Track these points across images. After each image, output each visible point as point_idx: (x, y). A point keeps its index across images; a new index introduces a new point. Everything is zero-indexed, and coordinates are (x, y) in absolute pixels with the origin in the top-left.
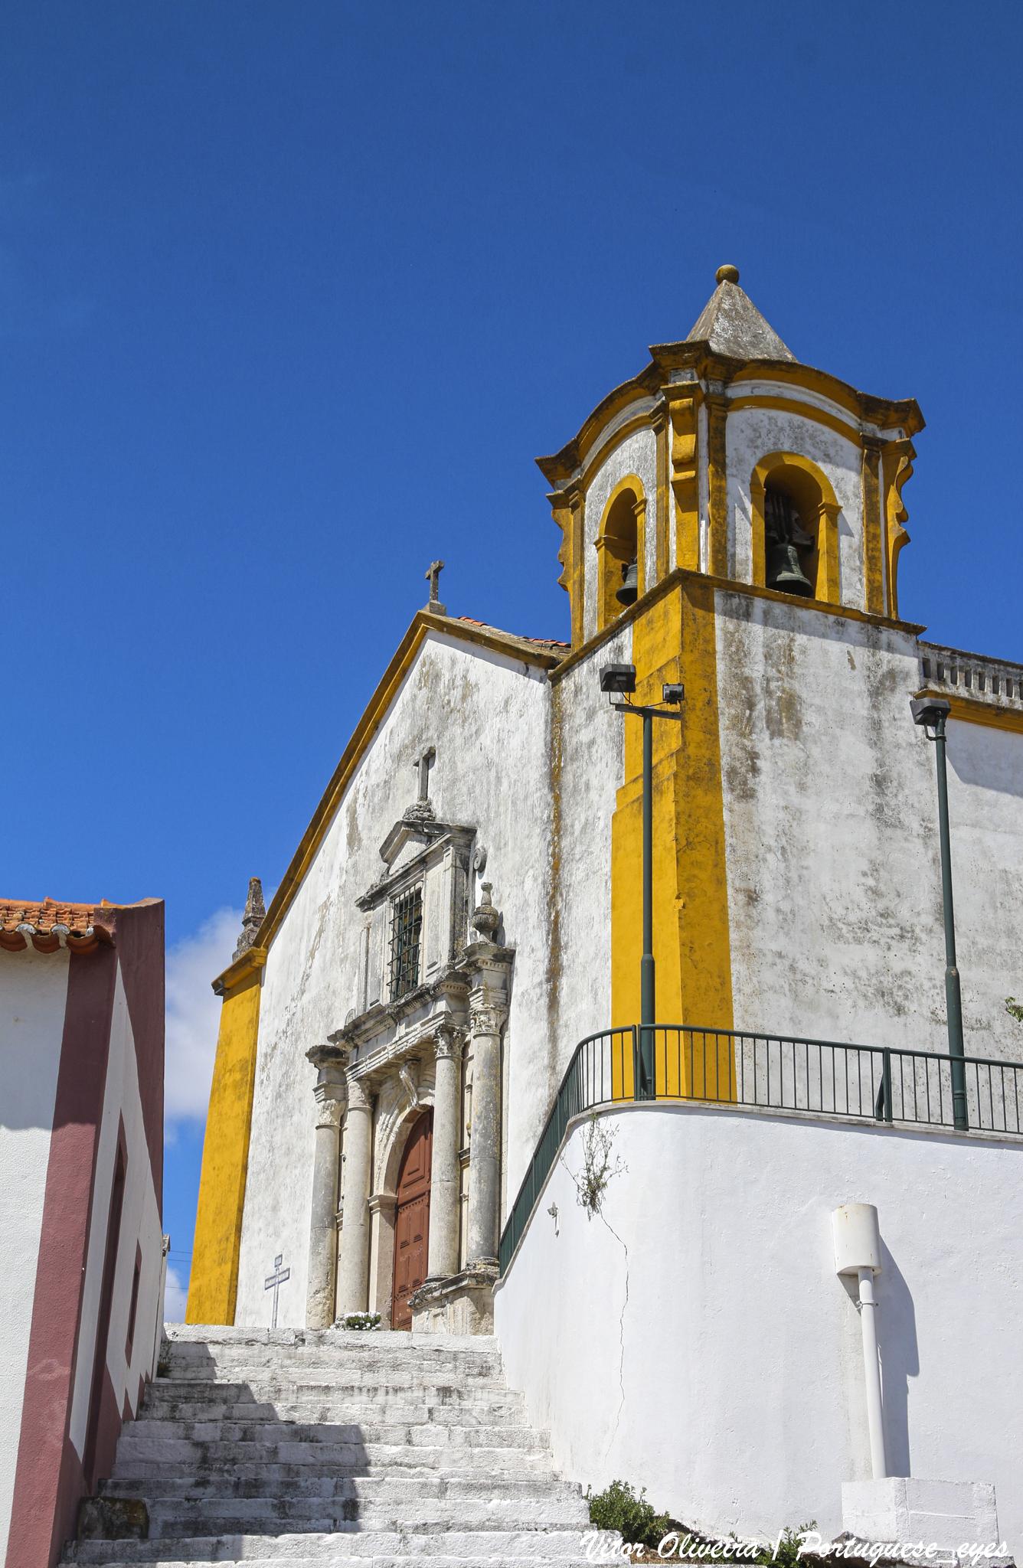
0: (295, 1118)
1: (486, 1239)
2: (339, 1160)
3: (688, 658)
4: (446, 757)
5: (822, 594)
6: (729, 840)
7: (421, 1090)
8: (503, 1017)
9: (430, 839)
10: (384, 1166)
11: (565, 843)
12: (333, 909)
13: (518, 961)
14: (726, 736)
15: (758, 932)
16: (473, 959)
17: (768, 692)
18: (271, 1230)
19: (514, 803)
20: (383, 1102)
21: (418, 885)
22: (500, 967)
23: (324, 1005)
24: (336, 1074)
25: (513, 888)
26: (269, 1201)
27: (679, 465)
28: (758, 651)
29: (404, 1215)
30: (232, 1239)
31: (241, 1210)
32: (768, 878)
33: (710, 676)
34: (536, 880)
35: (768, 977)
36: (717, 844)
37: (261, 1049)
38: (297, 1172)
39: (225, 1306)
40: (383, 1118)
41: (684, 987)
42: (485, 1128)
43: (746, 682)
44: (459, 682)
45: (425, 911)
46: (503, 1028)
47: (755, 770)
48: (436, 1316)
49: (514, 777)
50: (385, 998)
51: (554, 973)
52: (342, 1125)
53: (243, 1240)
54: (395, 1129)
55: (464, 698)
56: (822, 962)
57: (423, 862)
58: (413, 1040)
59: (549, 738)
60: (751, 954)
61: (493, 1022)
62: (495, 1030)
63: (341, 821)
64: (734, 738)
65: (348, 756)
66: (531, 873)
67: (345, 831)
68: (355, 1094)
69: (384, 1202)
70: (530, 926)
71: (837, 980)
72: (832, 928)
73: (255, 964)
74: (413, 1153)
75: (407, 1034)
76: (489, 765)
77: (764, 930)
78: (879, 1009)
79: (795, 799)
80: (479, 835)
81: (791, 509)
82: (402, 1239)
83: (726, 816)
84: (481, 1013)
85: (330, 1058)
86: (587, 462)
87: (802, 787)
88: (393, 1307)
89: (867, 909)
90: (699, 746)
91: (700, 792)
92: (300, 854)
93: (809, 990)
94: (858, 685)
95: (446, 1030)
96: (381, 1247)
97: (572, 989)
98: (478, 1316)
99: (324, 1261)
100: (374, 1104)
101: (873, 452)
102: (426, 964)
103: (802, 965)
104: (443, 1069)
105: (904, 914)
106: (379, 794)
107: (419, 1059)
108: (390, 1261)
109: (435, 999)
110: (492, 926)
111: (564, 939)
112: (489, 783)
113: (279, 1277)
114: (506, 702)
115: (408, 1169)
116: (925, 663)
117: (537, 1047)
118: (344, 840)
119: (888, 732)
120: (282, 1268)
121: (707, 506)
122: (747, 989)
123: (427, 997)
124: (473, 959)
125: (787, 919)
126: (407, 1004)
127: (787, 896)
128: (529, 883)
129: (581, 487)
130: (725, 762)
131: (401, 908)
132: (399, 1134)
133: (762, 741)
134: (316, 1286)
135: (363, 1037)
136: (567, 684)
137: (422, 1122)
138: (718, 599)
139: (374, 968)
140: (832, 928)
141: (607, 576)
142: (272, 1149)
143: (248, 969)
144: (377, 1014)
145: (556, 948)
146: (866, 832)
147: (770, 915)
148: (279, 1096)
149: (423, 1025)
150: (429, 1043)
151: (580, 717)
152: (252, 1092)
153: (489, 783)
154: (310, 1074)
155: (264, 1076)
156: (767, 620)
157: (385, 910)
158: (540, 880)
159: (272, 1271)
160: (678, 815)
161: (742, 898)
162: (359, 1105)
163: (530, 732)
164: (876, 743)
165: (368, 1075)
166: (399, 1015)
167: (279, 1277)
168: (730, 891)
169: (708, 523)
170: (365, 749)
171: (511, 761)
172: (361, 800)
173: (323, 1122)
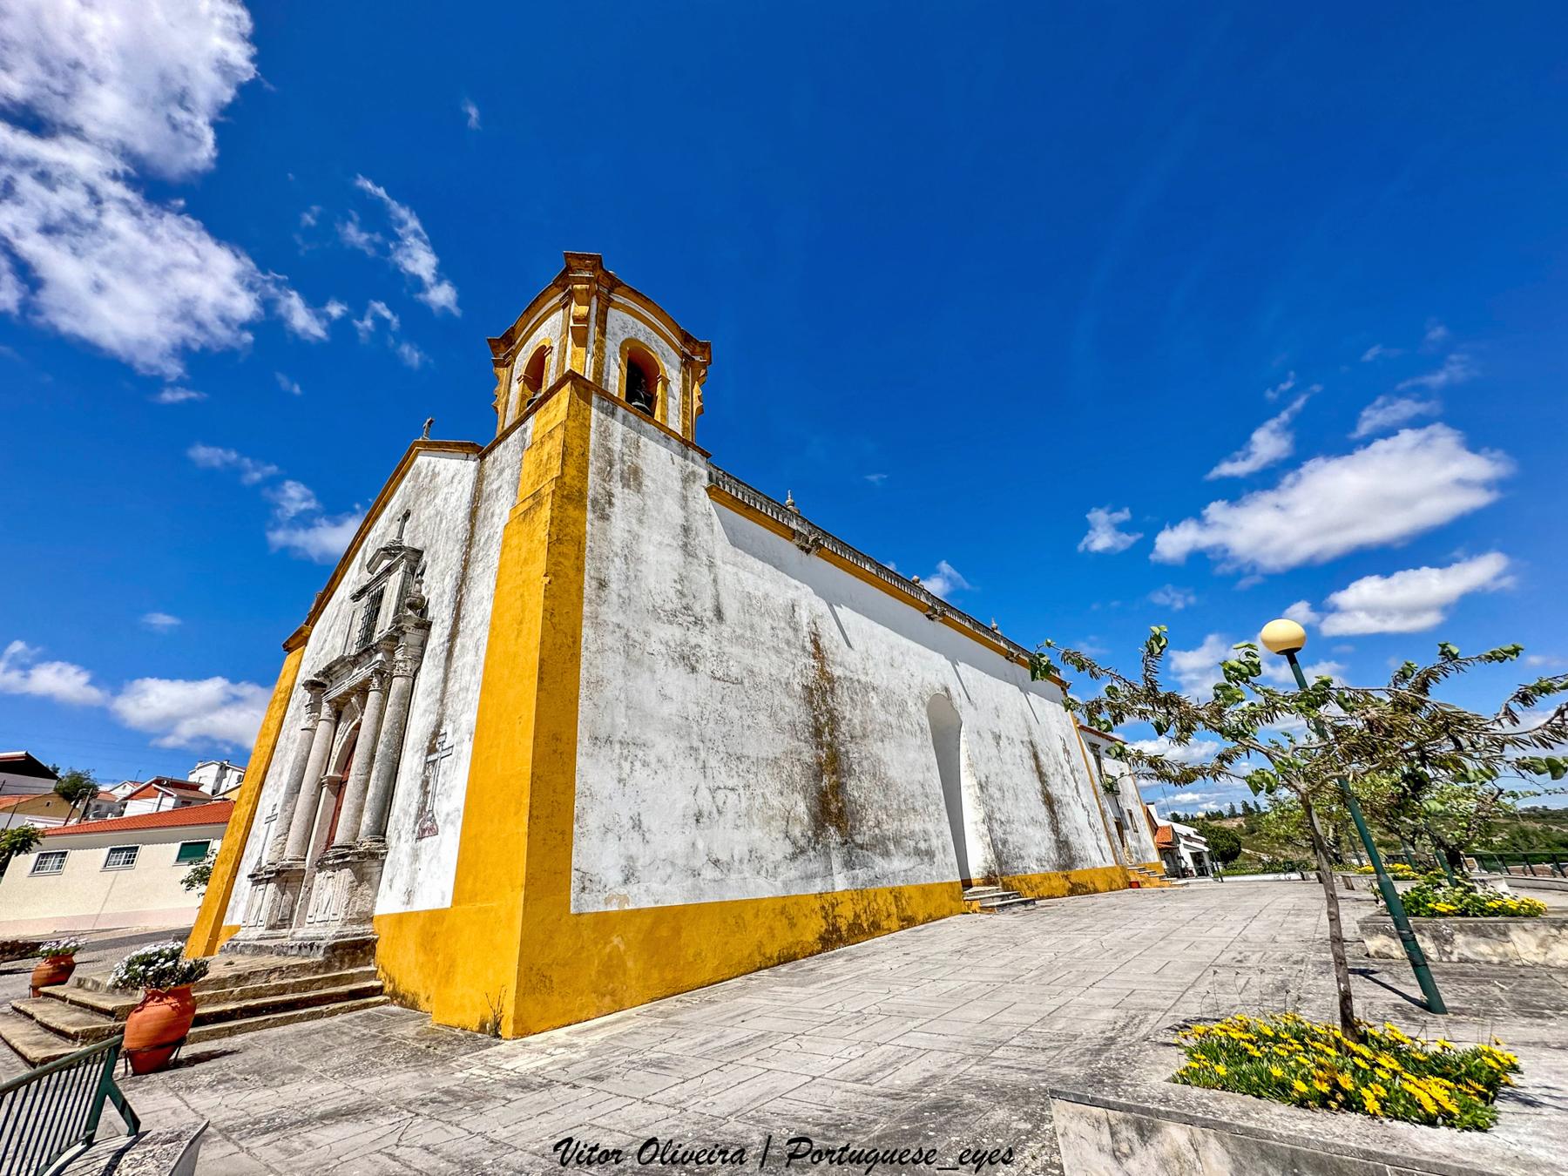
3: (570, 424)
5: (658, 417)
11: (474, 551)
14: (593, 479)
15: (604, 609)
17: (623, 462)
22: (420, 632)
25: (436, 587)
27: (576, 320)
28: (618, 436)
31: (265, 773)
32: (614, 572)
33: (586, 440)
35: (609, 640)
36: (580, 543)
41: (542, 643)
43: (609, 450)
47: (610, 504)
51: (453, 636)
56: (647, 634)
57: (389, 570)
60: (597, 624)
64: (598, 480)
68: (326, 710)
69: (331, 781)
71: (656, 647)
72: (654, 612)
76: (438, 513)
78: (681, 667)
79: (636, 527)
81: (642, 380)
83: (588, 527)
87: (640, 521)
89: (676, 604)
91: (570, 508)
93: (637, 652)
94: (676, 474)
95: (379, 672)
97: (463, 646)
100: (338, 716)
101: (687, 362)
104: (373, 696)
105: (697, 608)
107: (362, 690)
109: (377, 652)
110: (420, 606)
116: (710, 474)
119: (691, 503)
121: (592, 347)
122: (593, 648)
125: (626, 602)
128: (448, 578)
130: (590, 493)
133: (617, 488)
136: (490, 459)
138: (594, 398)
140: (654, 612)
141: (523, 397)
145: (457, 618)
146: (678, 557)
147: (614, 598)
150: (368, 681)
151: (495, 474)
156: (625, 421)
160: (552, 519)
161: (594, 584)
164: (684, 507)
166: (355, 661)
168: (586, 577)
170: (377, 517)
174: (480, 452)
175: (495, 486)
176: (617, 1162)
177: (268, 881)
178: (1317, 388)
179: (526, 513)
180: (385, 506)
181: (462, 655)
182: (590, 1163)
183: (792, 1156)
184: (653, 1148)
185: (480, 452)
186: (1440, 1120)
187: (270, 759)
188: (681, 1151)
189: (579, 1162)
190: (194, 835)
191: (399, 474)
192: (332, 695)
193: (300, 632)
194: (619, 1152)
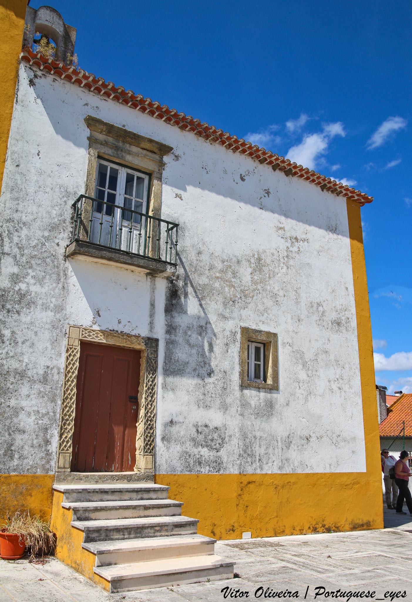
176: (247, 596)
178: (336, 129)
182: (336, 597)
183: (317, 594)
184: (260, 591)
186: (38, 516)
188: (273, 592)
189: (266, 597)
194: (248, 593)
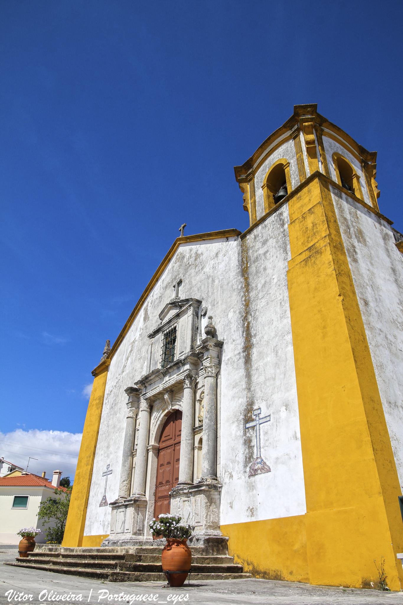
0: (117, 415)
1: (211, 467)
2: (135, 430)
4: (187, 281)
6: (353, 277)
7: (173, 403)
8: (218, 370)
9: (181, 307)
10: (155, 433)
11: (252, 294)
12: (136, 343)
13: (225, 347)
16: (206, 344)
18: (106, 455)
19: (221, 287)
20: (155, 408)
21: (175, 325)
22: (217, 349)
23: (131, 375)
24: (136, 399)
26: (106, 444)
29: (162, 453)
30: (92, 457)
31: (95, 447)
32: (369, 295)
33: (334, 212)
34: (235, 312)
37: (107, 392)
38: (117, 434)
39: (87, 480)
40: (155, 414)
42: (210, 417)
43: (345, 219)
44: (193, 255)
45: (178, 334)
46: (218, 374)
48: (184, 501)
49: (221, 278)
50: (159, 367)
51: (248, 347)
52: (136, 417)
53: (96, 457)
54: (160, 419)
55: (196, 260)
57: (178, 316)
58: (172, 382)
59: (240, 259)
60: (372, 329)
61: (214, 372)
62: (214, 375)
63: (142, 313)
65: (146, 291)
66: (232, 310)
67: (143, 316)
68: (144, 405)
69: (154, 448)
70: (232, 331)
73: (106, 365)
74: (167, 428)
75: (169, 380)
76: (208, 278)
77: (373, 318)
80: (203, 303)
82: (161, 462)
84: (209, 367)
85: (134, 393)
86: (255, 166)
87: (372, 264)
88: (156, 490)
90: (335, 235)
92: (126, 326)
95: (189, 376)
96: (152, 466)
98: (209, 504)
99: (127, 469)
100: (151, 408)
102: (178, 352)
103: (389, 337)
104: (187, 393)
106: (157, 301)
107: (175, 391)
108: (155, 472)
109: (184, 365)
111: (253, 332)
112: (208, 284)
113: (108, 472)
114: (217, 254)
115: (163, 436)
117: (238, 381)
118: (142, 319)
120: (110, 469)
122: (373, 344)
123: (179, 364)
124: (206, 344)
126: (170, 367)
127: (377, 306)
128: (231, 315)
129: (253, 173)
131: (167, 336)
132: (162, 421)
134: (124, 479)
135: (149, 383)
137: (175, 416)
139: (154, 358)
142: (108, 426)
143: (104, 366)
144: (156, 372)
148: (112, 408)
149: (177, 375)
152: (102, 407)
153: (208, 284)
154: (125, 398)
155: (107, 401)
156: (347, 202)
157: (160, 336)
158: (237, 312)
159: (105, 470)
162: (146, 409)
163: (230, 259)
165: (150, 398)
166: (166, 372)
167: (108, 472)
169: (322, 163)
171: (219, 273)
172: (150, 304)
173: (129, 416)
174: (241, 234)
175: (261, 251)
177: (126, 506)
179: (306, 261)
180: (157, 280)
181: (261, 355)
185: (241, 234)
187: (97, 439)
190: (21, 491)
191: (167, 260)
192: (148, 395)
193: (104, 363)
